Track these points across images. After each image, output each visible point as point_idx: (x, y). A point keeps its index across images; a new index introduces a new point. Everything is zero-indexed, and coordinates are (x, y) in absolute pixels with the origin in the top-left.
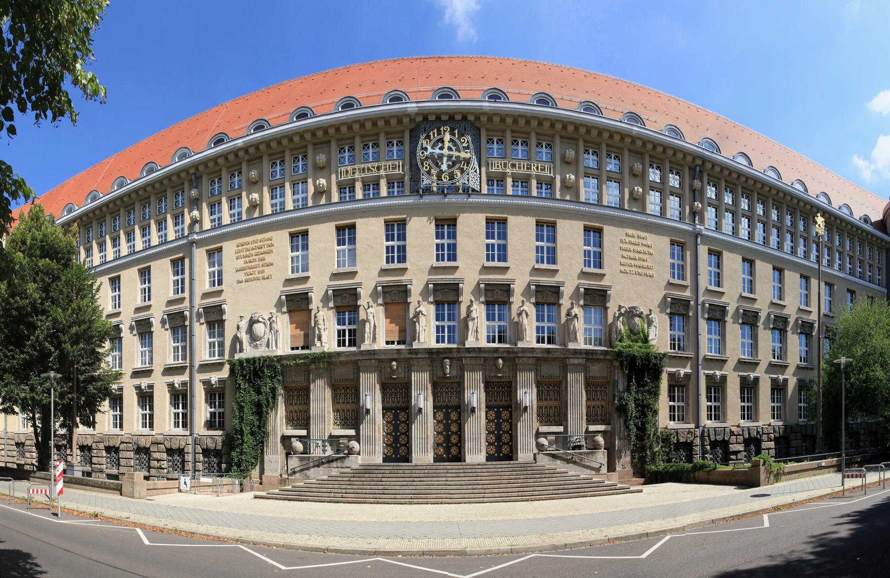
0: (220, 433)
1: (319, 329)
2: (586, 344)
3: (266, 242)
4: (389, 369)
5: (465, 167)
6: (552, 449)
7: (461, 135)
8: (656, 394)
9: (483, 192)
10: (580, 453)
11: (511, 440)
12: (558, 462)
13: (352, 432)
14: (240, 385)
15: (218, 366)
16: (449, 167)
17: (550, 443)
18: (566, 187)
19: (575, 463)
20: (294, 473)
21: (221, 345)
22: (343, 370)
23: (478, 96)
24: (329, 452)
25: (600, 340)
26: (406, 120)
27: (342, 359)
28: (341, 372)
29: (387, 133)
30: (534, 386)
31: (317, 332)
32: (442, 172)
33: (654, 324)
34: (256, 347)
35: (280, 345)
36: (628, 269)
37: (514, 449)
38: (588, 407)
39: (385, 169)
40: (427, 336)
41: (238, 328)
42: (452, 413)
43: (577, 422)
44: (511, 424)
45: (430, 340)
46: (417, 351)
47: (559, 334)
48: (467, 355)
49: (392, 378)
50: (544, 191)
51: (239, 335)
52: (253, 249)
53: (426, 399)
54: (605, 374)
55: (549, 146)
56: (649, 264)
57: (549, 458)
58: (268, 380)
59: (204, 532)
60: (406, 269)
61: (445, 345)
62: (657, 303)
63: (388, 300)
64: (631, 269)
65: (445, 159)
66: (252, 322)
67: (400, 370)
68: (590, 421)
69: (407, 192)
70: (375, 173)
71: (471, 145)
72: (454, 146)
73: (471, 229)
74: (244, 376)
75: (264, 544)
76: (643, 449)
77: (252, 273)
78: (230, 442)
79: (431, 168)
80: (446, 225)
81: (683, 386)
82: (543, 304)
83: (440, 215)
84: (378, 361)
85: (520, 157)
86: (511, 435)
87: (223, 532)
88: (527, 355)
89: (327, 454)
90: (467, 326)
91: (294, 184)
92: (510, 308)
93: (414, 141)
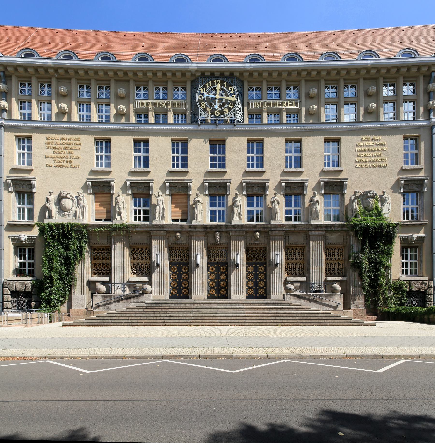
0: (30, 278)
1: (119, 208)
2: (325, 220)
3: (74, 142)
4: (174, 238)
5: (232, 107)
6: (298, 293)
7: (229, 85)
8: (389, 254)
9: (245, 123)
10: (320, 296)
11: (265, 285)
12: (303, 301)
13: (146, 279)
14: (49, 243)
15: (29, 227)
16: (220, 106)
17: (295, 288)
18: (309, 114)
19: (316, 302)
20: (99, 306)
21: (31, 211)
22: (139, 237)
23: (243, 60)
24: (127, 292)
25: (338, 217)
26: (188, 75)
27: (138, 229)
28: (137, 239)
29: (173, 82)
30: (283, 250)
31: (118, 210)
32: (215, 110)
33: (388, 202)
34: (65, 216)
35: (86, 216)
36: (362, 164)
37: (268, 292)
38: (327, 264)
39: (172, 105)
40: (203, 216)
41: (47, 200)
42: (221, 268)
43: (318, 274)
44: (265, 275)
45: (205, 220)
46: (195, 227)
47: (303, 215)
48: (233, 229)
49: (176, 244)
50: (292, 119)
51: (48, 205)
52: (62, 144)
53: (202, 258)
54: (341, 241)
55: (296, 88)
56: (382, 158)
57: (295, 298)
58: (76, 241)
59: (10, 355)
60: (188, 172)
61: (217, 223)
62: (390, 185)
63: (174, 192)
64: (365, 164)
65: (217, 102)
66: (60, 198)
67: (183, 238)
68: (328, 273)
69: (189, 122)
70: (164, 107)
71: (236, 92)
72: (224, 93)
73: (237, 149)
74: (54, 237)
75: (71, 357)
76: (376, 294)
77: (58, 161)
78: (39, 286)
79: (206, 107)
80: (218, 145)
81: (416, 247)
82: (291, 195)
83: (213, 138)
84: (166, 232)
85: (273, 98)
86: (265, 283)
87: (29, 353)
88: (277, 229)
89: (126, 293)
90: (233, 211)
91: (99, 104)
92: (265, 199)
93: (194, 88)
